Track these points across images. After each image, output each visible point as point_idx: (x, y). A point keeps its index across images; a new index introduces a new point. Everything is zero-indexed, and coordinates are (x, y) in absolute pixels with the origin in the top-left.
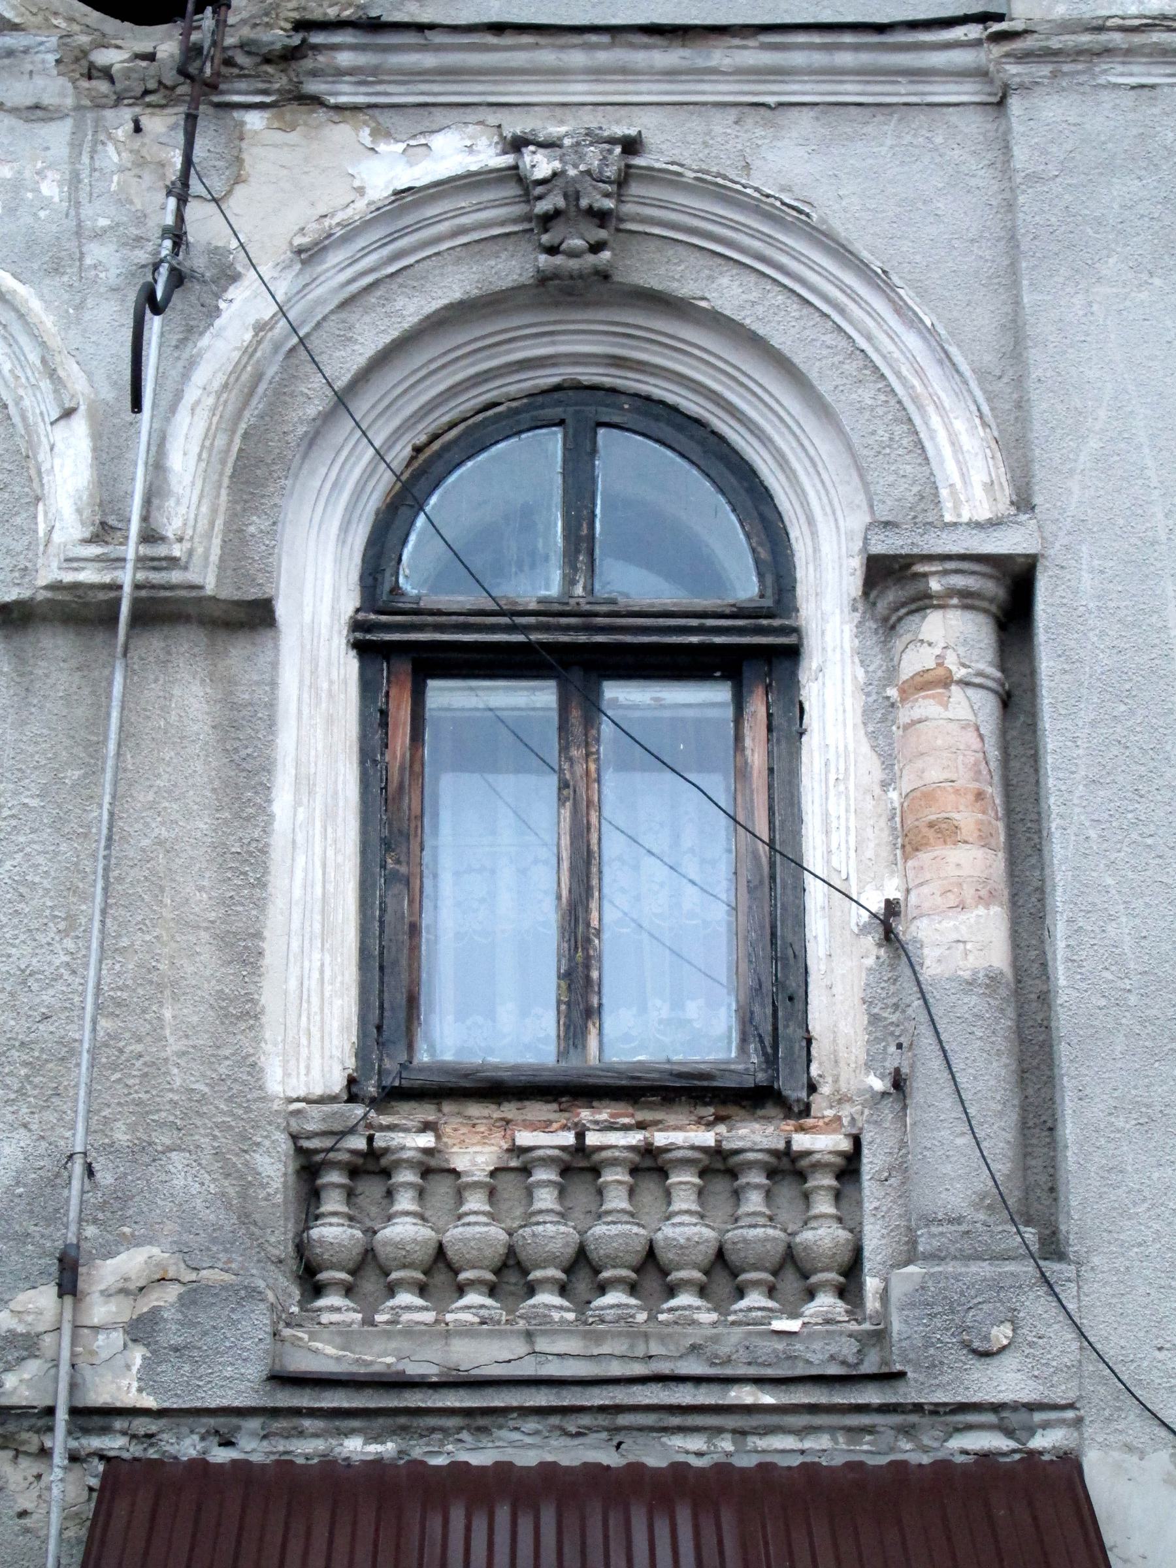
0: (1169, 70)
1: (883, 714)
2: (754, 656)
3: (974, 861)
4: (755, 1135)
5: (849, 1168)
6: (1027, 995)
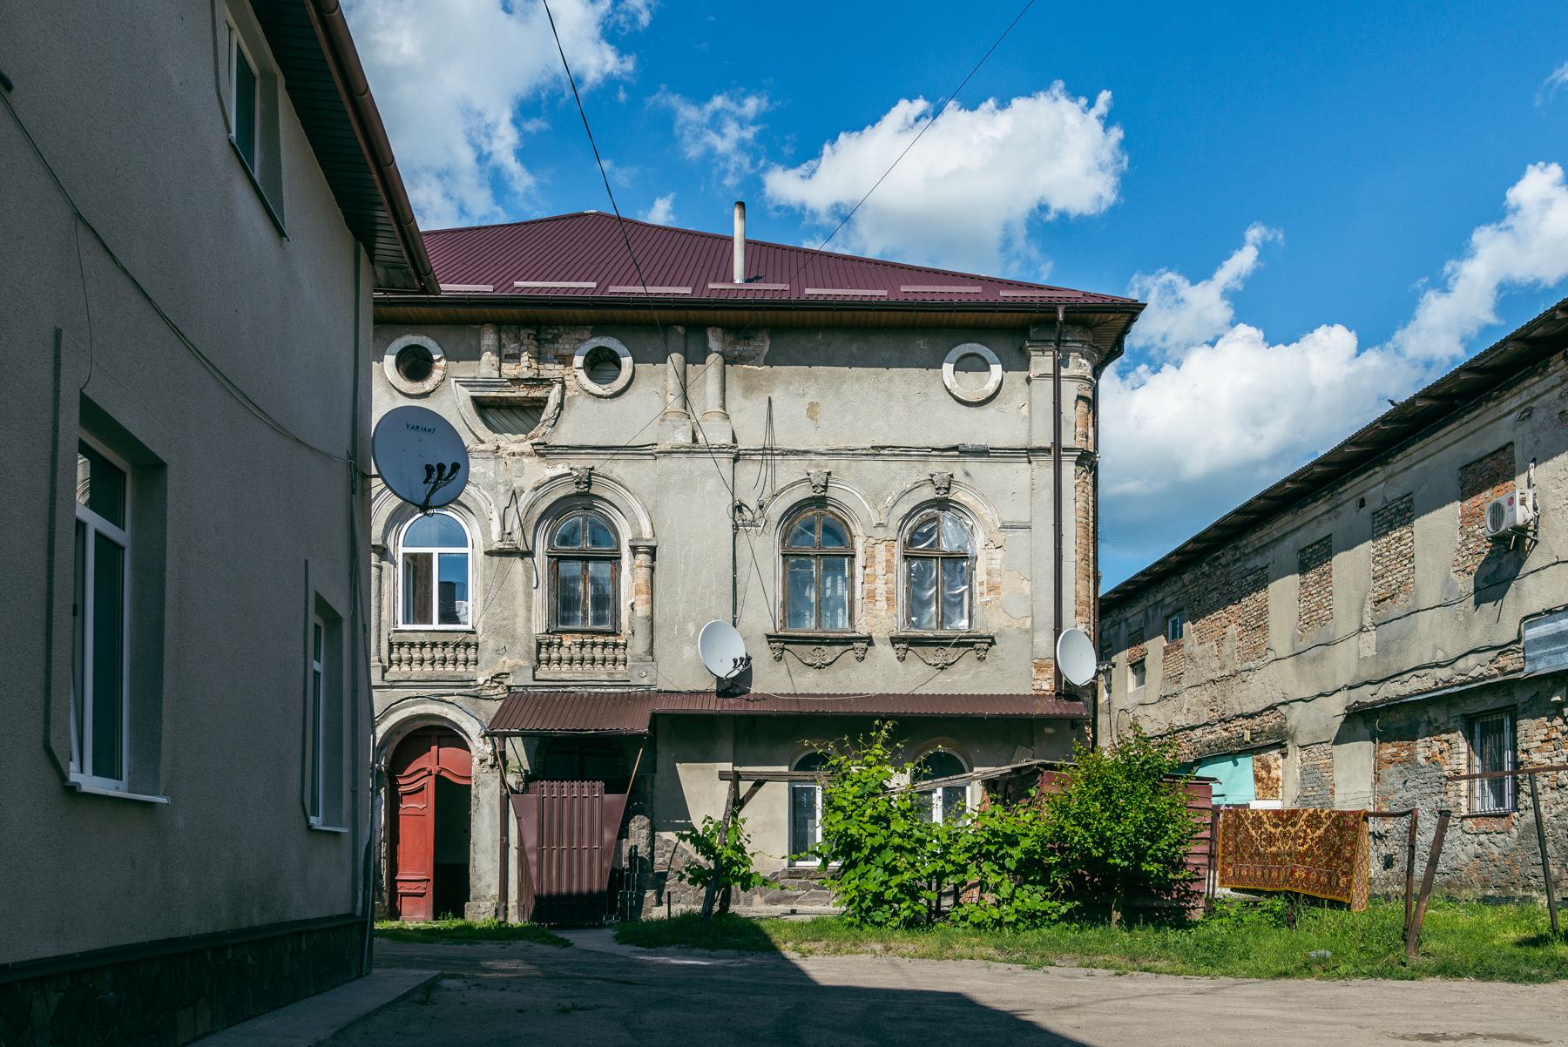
1: (632, 570)
2: (615, 559)
3: (645, 597)
4: (611, 639)
5: (625, 645)
6: (651, 619)
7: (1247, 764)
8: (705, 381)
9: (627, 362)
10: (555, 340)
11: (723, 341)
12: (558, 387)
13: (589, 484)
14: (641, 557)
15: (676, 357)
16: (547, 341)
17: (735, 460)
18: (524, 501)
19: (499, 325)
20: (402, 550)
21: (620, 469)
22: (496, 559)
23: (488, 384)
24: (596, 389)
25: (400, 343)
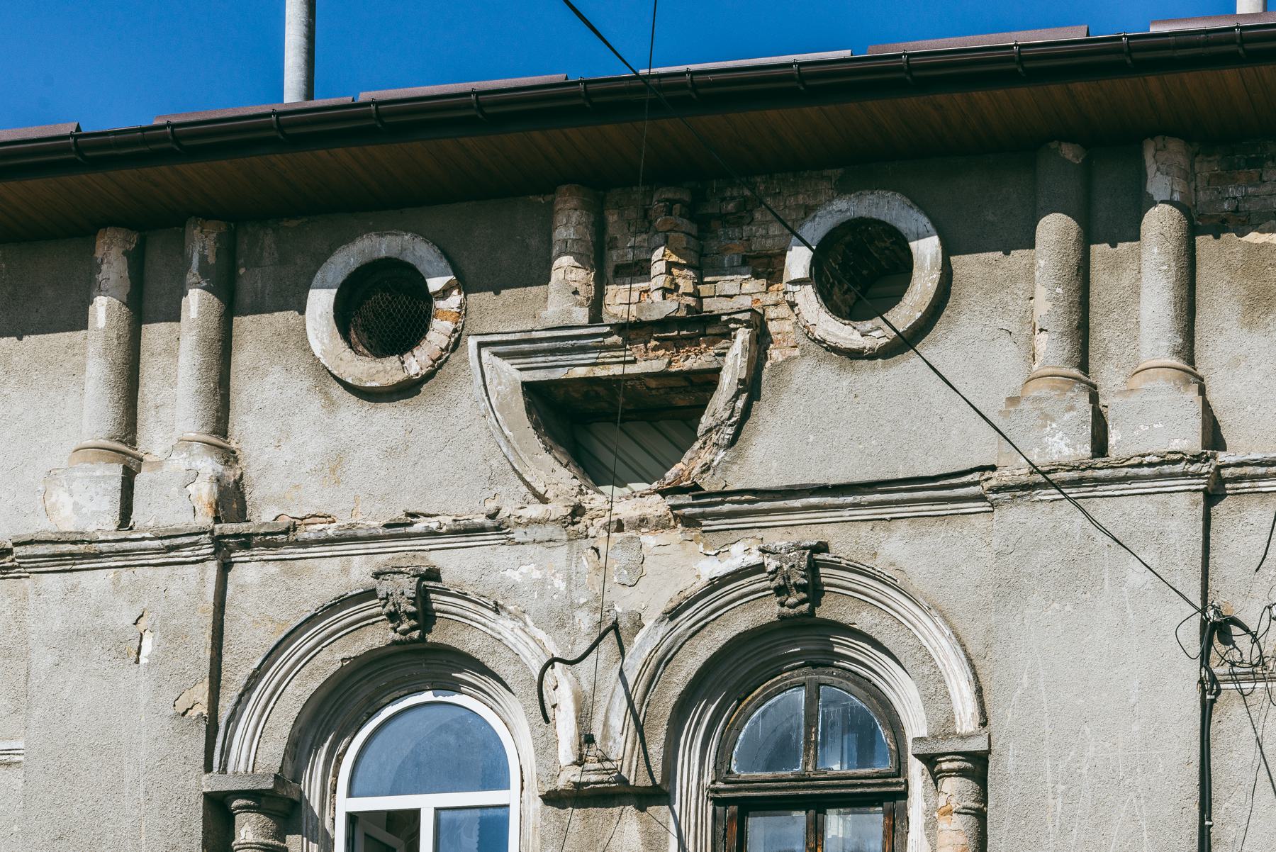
0: (534, 842)
1: (931, 827)
2: (890, 799)
7: (800, 816)
8: (1136, 290)
9: (926, 250)
10: (742, 216)
11: (1189, 176)
12: (743, 335)
13: (814, 591)
14: (951, 785)
15: (1054, 229)
16: (724, 219)
17: (1212, 497)
18: (642, 647)
19: (601, 185)
20: (345, 804)
21: (897, 545)
22: (574, 816)
23: (563, 344)
24: (845, 334)
25: (345, 261)
